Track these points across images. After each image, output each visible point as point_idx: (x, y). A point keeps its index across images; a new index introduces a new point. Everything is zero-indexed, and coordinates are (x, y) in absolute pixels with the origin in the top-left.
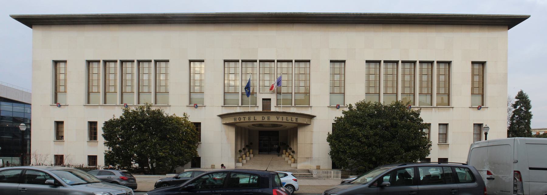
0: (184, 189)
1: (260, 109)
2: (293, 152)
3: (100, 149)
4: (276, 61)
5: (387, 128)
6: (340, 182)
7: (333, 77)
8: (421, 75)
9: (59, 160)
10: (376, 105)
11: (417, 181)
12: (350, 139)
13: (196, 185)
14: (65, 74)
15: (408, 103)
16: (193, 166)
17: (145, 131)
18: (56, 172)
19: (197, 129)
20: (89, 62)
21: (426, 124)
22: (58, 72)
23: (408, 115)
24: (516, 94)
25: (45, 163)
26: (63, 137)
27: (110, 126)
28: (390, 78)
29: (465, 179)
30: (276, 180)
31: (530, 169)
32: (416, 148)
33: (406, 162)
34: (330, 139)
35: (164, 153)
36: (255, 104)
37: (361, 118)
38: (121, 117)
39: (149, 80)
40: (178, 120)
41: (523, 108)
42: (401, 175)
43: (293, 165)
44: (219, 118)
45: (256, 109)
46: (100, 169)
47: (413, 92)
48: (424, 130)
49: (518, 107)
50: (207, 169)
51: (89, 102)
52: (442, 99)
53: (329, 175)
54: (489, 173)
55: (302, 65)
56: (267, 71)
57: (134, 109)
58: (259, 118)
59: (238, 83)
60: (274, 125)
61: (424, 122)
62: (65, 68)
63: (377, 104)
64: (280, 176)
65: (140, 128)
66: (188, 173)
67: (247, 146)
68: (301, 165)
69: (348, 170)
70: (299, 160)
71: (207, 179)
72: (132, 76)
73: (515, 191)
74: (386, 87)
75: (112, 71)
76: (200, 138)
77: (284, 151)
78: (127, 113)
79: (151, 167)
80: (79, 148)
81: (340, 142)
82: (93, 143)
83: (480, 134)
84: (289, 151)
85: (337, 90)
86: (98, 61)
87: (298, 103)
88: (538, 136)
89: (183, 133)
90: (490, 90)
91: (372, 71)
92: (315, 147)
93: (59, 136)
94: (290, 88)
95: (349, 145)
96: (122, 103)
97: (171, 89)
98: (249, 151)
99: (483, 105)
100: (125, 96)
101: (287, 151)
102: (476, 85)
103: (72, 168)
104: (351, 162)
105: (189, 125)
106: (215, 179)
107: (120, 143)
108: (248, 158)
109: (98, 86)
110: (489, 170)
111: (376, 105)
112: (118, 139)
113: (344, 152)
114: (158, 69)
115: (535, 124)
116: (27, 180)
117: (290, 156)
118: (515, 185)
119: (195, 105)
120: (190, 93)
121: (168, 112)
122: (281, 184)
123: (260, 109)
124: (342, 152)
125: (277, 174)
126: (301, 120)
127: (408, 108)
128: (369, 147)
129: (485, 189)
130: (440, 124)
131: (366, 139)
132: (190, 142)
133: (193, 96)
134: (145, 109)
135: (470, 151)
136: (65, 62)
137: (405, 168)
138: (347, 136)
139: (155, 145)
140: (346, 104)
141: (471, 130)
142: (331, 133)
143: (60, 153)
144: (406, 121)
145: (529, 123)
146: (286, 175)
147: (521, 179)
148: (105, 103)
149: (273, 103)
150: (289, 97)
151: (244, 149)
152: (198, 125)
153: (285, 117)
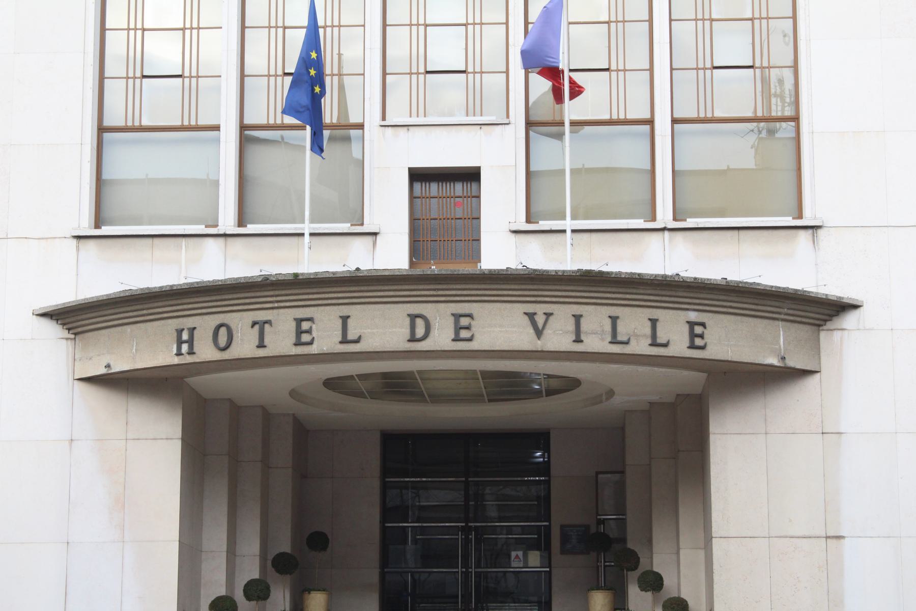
1: (393, 254)
34: (278, 555)
44: (52, 329)
45: (355, 258)
58: (382, 329)
59: (217, 51)
60: (509, 386)
67: (282, 564)
87: (699, 205)
123: (393, 254)
126: (733, 340)
150: (626, 151)
153: (596, 319)
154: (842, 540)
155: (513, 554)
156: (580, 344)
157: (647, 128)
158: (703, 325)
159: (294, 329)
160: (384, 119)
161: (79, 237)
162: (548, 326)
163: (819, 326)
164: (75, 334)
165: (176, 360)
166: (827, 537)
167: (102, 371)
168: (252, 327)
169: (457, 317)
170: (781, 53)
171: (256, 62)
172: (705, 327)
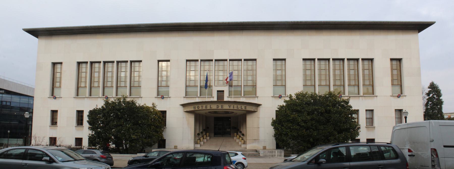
0: (152, 166)
1: (215, 99)
2: (243, 135)
3: (85, 132)
4: (228, 60)
5: (322, 114)
6: (283, 160)
7: (276, 72)
8: (349, 70)
9: (53, 141)
10: (312, 95)
11: (349, 158)
12: (291, 123)
13: (162, 163)
14: (61, 73)
15: (339, 93)
16: (159, 147)
17: (120, 118)
18: (51, 151)
19: (163, 116)
20: (79, 63)
21: (355, 110)
22: (55, 71)
23: (339, 103)
24: (428, 85)
25: (42, 144)
26: (56, 122)
27: (93, 114)
28: (323, 72)
29: (390, 156)
30: (227, 158)
31: (445, 146)
32: (347, 130)
33: (339, 142)
34: (274, 123)
35: (136, 136)
36: (211, 95)
37: (300, 105)
38: (102, 107)
39: (126, 77)
40: (148, 108)
41: (435, 96)
42: (335, 154)
43: (243, 146)
44: (181, 106)
45: (212, 100)
46: (85, 149)
47: (343, 84)
48: (354, 116)
49: (431, 95)
50: (171, 149)
51: (77, 95)
52: (368, 89)
53: (274, 154)
54: (409, 151)
55: (250, 63)
56: (221, 68)
57: (112, 100)
58: (214, 107)
59: (198, 77)
60: (227, 112)
61: (353, 109)
62: (61, 68)
63: (313, 94)
64: (230, 155)
65: (117, 115)
66: (155, 153)
67: (204, 130)
68: (250, 146)
69: (289, 149)
70: (248, 142)
71: (171, 157)
72: (112, 74)
73: (433, 166)
74: (320, 80)
75: (97, 70)
76: (166, 124)
77: (235, 134)
78: (107, 103)
79: (125, 148)
80: (69, 132)
81: (282, 126)
82: (80, 128)
83: (401, 118)
84: (239, 134)
85: (279, 83)
86: (86, 63)
87: (246, 94)
88: (450, 119)
89: (151, 119)
90: (407, 81)
91: (308, 67)
92: (262, 131)
93: (54, 122)
94: (240, 82)
95: (290, 128)
96: (103, 95)
97: (143, 85)
98: (206, 134)
99: (402, 94)
100: (106, 89)
101: (237, 134)
102: (395, 78)
103: (63, 148)
104: (292, 142)
105: (156, 113)
106: (175, 159)
107: (101, 128)
108: (205, 140)
109: (86, 82)
110: (410, 148)
111: (312, 95)
112: (100, 124)
113: (286, 135)
114: (132, 67)
115: (446, 109)
116: (28, 157)
117: (241, 138)
118: (433, 161)
119: (161, 96)
120: (158, 86)
121: (140, 102)
122: (232, 162)
123: (215, 99)
124: (285, 134)
125: (228, 153)
126: (249, 108)
127: (339, 97)
128: (307, 130)
129: (407, 165)
130: (366, 110)
131: (304, 123)
132: (157, 127)
133: (160, 89)
134: (122, 100)
135: (393, 132)
136: (61, 63)
137: (338, 148)
138: (288, 121)
139: (129, 129)
140: (287, 94)
141: (393, 114)
142: (275, 119)
143: (54, 136)
144: (338, 108)
145: (441, 108)
146: (236, 154)
147: (437, 155)
148: (90, 95)
149: (226, 94)
150: (239, 89)
151: (202, 133)
152: (164, 113)
153: (235, 106)
170: (255, 74)
171: (202, 79)
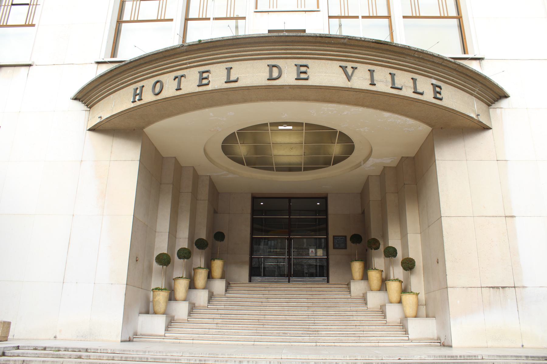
44: (79, 106)
154: (514, 218)
155: (311, 250)
156: (374, 86)
157: (387, 20)
158: (440, 87)
159: (198, 78)
160: (256, 8)
161: (98, 63)
162: (354, 74)
163: (489, 105)
164: (90, 108)
165: (133, 105)
166: (506, 217)
167: (98, 120)
168: (174, 79)
169: (298, 66)
172: (441, 89)
